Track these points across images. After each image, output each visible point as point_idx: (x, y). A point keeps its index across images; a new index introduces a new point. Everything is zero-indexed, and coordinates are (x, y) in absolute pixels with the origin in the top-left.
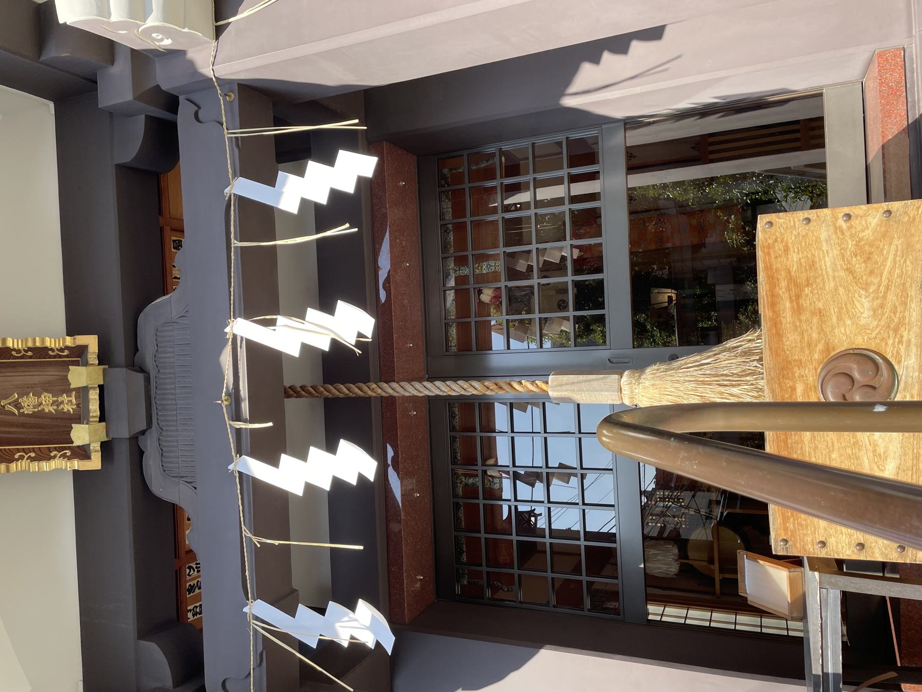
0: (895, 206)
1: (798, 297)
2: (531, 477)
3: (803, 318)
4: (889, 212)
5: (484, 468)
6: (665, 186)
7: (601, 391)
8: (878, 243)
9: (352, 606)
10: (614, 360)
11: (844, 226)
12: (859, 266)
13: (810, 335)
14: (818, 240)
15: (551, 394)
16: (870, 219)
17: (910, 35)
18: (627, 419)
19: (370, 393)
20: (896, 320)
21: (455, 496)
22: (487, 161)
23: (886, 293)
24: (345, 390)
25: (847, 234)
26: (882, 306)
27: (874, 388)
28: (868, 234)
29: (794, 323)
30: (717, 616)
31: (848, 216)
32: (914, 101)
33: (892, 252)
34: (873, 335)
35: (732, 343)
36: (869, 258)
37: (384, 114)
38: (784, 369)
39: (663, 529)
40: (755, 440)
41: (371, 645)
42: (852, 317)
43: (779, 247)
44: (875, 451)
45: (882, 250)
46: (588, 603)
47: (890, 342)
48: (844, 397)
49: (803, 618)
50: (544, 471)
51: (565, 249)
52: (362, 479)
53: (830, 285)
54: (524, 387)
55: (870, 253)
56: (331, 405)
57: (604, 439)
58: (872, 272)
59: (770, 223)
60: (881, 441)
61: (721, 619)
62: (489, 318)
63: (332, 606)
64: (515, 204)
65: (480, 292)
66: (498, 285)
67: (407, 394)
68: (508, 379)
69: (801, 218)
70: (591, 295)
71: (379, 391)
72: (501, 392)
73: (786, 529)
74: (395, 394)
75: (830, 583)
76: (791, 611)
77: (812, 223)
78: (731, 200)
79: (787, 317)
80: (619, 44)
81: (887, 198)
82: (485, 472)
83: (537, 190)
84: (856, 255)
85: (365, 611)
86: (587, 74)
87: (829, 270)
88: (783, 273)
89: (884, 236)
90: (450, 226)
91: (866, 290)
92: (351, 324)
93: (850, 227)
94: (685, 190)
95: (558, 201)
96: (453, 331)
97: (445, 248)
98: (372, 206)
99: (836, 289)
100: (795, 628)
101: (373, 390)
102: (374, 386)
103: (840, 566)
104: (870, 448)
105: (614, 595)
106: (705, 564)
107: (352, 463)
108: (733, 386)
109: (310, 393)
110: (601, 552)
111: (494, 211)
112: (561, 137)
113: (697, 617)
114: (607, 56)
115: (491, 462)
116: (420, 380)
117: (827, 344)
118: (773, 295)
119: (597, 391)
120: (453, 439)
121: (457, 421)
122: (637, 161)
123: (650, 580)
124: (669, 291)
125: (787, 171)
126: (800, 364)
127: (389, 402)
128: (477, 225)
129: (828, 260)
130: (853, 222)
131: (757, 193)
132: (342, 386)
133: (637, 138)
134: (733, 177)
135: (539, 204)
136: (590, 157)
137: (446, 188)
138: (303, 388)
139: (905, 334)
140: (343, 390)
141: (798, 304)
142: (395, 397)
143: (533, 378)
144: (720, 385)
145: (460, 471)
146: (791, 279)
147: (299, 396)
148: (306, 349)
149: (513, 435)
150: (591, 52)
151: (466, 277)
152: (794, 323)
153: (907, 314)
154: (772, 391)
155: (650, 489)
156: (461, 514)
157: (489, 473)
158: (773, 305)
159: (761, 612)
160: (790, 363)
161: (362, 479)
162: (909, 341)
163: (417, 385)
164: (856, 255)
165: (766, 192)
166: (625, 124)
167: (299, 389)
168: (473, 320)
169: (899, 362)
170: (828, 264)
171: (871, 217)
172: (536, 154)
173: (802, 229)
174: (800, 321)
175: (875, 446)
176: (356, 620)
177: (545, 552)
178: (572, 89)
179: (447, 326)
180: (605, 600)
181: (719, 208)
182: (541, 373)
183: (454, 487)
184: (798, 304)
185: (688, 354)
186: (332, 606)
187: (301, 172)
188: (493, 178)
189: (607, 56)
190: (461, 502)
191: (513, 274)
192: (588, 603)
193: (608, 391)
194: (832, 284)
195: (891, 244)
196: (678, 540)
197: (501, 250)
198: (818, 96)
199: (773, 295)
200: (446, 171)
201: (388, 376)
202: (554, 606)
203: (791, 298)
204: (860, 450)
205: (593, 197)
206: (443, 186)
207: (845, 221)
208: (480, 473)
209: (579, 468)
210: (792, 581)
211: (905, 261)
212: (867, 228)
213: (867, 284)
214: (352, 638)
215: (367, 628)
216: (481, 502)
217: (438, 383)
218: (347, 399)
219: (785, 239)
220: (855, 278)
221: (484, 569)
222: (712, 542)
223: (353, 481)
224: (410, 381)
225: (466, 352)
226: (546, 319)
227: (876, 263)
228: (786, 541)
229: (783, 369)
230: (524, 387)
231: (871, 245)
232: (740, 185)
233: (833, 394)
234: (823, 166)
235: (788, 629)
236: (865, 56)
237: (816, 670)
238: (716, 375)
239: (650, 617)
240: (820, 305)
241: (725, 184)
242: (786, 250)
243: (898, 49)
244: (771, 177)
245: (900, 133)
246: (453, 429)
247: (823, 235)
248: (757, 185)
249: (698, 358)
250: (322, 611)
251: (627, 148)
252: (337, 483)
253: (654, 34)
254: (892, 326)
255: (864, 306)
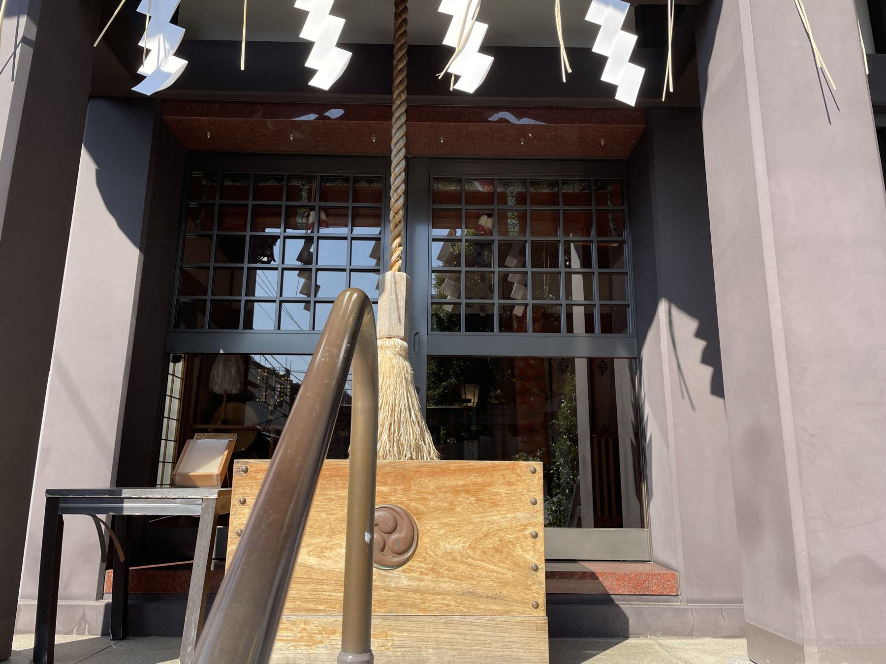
0: (542, 575)
1: (467, 492)
2: (306, 257)
3: (448, 495)
4: (536, 569)
5: (317, 208)
6: (573, 400)
7: (390, 320)
8: (510, 559)
9: (179, 53)
10: (417, 338)
11: (527, 532)
12: (490, 543)
13: (432, 499)
14: (516, 510)
15: (389, 274)
16: (531, 553)
17: (688, 601)
18: (366, 318)
19: (396, 93)
20: (441, 571)
21: (290, 178)
22: (615, 229)
23: (466, 563)
24: (401, 66)
25: (520, 535)
26: (454, 559)
27: (382, 550)
28: (519, 551)
29: (444, 487)
30: (173, 424)
31: (535, 536)
32: (630, 601)
33: (501, 570)
34: (428, 550)
35: (428, 437)
36: (497, 551)
37: (674, 119)
38: (403, 477)
39: (255, 386)
40: (338, 447)
41: (142, 70)
42: (446, 535)
43: (513, 478)
44: (326, 548)
45: (503, 562)
46: (185, 299)
47: (423, 565)
48: (377, 525)
49: (173, 485)
50: (313, 267)
51: (523, 299)
52: (312, 72)
53: (475, 518)
54: (396, 249)
55: (501, 552)
56: (385, 52)
57: (348, 293)
58: (484, 553)
59: (534, 472)
60: (336, 553)
61: (171, 427)
62: (463, 226)
63: (179, 32)
64: (570, 260)
65: (490, 216)
66: (495, 233)
67: (394, 131)
68: (403, 233)
69: (537, 498)
70: (479, 322)
71: (398, 102)
72: (392, 226)
73: (257, 471)
74: (394, 119)
75: (207, 507)
76: (181, 475)
77: (531, 506)
78: (555, 457)
79: (449, 482)
80: (712, 357)
81: (549, 575)
82: (313, 209)
83: (581, 276)
84: (500, 541)
85: (177, 66)
86: (687, 325)
87: (489, 518)
88: (489, 480)
89: (517, 564)
90: (556, 190)
91: (469, 547)
92: (469, 70)
93: (525, 537)
94: (567, 417)
95: (569, 293)
96: (453, 187)
97: (535, 183)
98: (583, 109)
99: (471, 523)
100: (165, 471)
101: (399, 95)
102: (403, 97)
103: (222, 520)
104: (329, 545)
105: (192, 324)
106: (222, 417)
107: (328, 66)
108: (389, 436)
109: (398, 29)
110: (234, 315)
111: (566, 234)
112: (630, 300)
113: (173, 407)
114: (701, 344)
115: (323, 216)
116: (407, 146)
117: (423, 513)
118: (469, 470)
119: (390, 316)
120: (346, 180)
121: (364, 185)
122: (600, 368)
123: (210, 359)
124: (476, 401)
125: (577, 502)
126: (407, 490)
127: (386, 114)
128: (555, 219)
129: (498, 518)
130: (530, 541)
131: (559, 479)
132: (405, 63)
133: (621, 369)
134: (576, 458)
135: (568, 276)
136: (607, 328)
137: (593, 188)
138: (405, 21)
139: (429, 577)
140: (401, 64)
141: (461, 491)
142: (391, 120)
143: (403, 257)
144: (391, 424)
145: (314, 186)
146: (482, 487)
147: (397, 16)
148: (447, 20)
149: (349, 239)
150: (708, 331)
151: (506, 203)
152: (444, 487)
153: (446, 579)
154: (384, 466)
155: (292, 378)
156: (272, 183)
157: (312, 213)
158: (461, 470)
159: (175, 463)
160: (409, 482)
161: (312, 72)
162: (423, 580)
163: (403, 142)
164: (500, 541)
165: (558, 486)
166: (635, 358)
167: (404, 17)
168: (463, 206)
169: (404, 571)
170: (494, 518)
171: (534, 554)
172: (614, 277)
173: (528, 498)
174: (445, 492)
175: (331, 549)
176: (166, 57)
177: (231, 295)
178: (675, 311)
179: (459, 181)
180: (188, 317)
181: (548, 446)
182: (408, 266)
183: (300, 178)
184: (461, 491)
185: (420, 400)
186: (179, 32)
187: (626, 27)
188: (599, 234)
189: (701, 344)
190: (284, 183)
191: (506, 249)
192: (185, 299)
193: (390, 326)
194: (476, 520)
195: (509, 569)
196: (245, 396)
197: (528, 237)
198: (642, 523)
199: (469, 470)
200: (610, 188)
201: (412, 114)
202: (178, 300)
203: (466, 485)
204: (328, 536)
205: (570, 330)
206: (596, 185)
207: (531, 533)
208: (312, 204)
209: (316, 299)
210: (209, 477)
211: (492, 580)
212: (524, 551)
213: (475, 548)
214: (148, 51)
215: (159, 67)
216: (284, 203)
217: (403, 164)
218: (391, 68)
219: (520, 483)
220: (481, 539)
221: (218, 202)
222: (242, 423)
223: (309, 64)
224: (407, 135)
225: (433, 203)
226: (458, 280)
227: (493, 557)
228: (246, 471)
229: (403, 476)
230: (396, 249)
231: (508, 553)
232: (567, 464)
233: (379, 516)
234: (579, 525)
235: (164, 462)
236: (673, 563)
237: (126, 492)
238: (399, 423)
239: (171, 364)
240: (459, 509)
241: (569, 453)
242: (510, 484)
243: (677, 590)
244: (571, 491)
245: (604, 588)
246: (356, 180)
247: (520, 515)
248: (566, 479)
249: (416, 407)
250: (175, 20)
251: (612, 360)
252: (307, 46)
253: (717, 388)
254: (436, 567)
255: (455, 545)
